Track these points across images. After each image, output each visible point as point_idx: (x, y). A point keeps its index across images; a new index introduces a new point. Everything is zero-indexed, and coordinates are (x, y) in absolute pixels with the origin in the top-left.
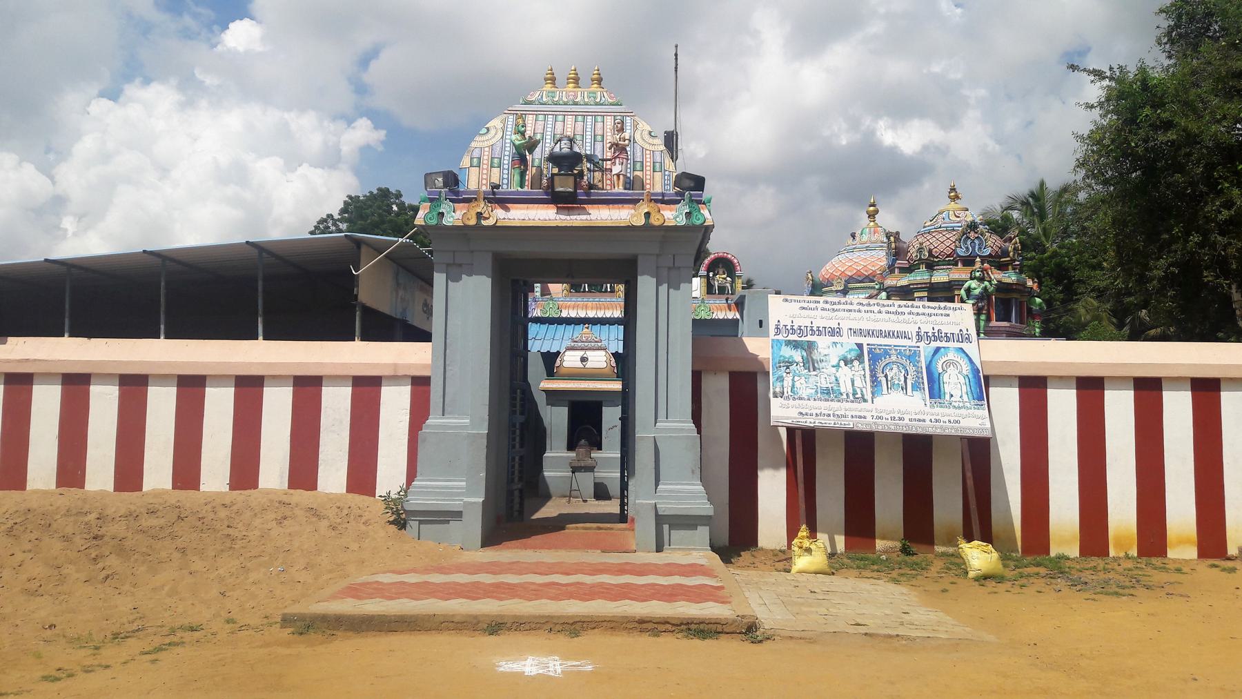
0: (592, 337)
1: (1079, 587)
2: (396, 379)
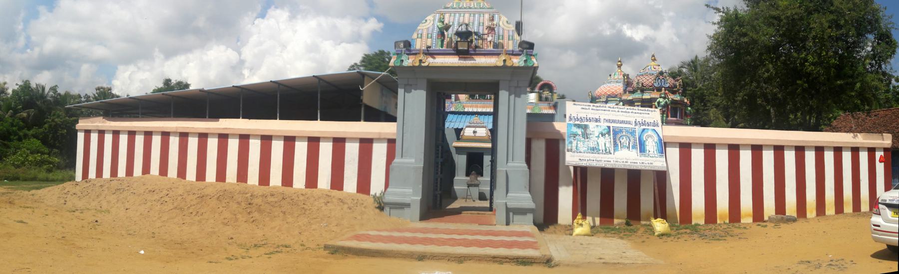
0: (479, 121)
1: (703, 238)
2: (380, 140)
